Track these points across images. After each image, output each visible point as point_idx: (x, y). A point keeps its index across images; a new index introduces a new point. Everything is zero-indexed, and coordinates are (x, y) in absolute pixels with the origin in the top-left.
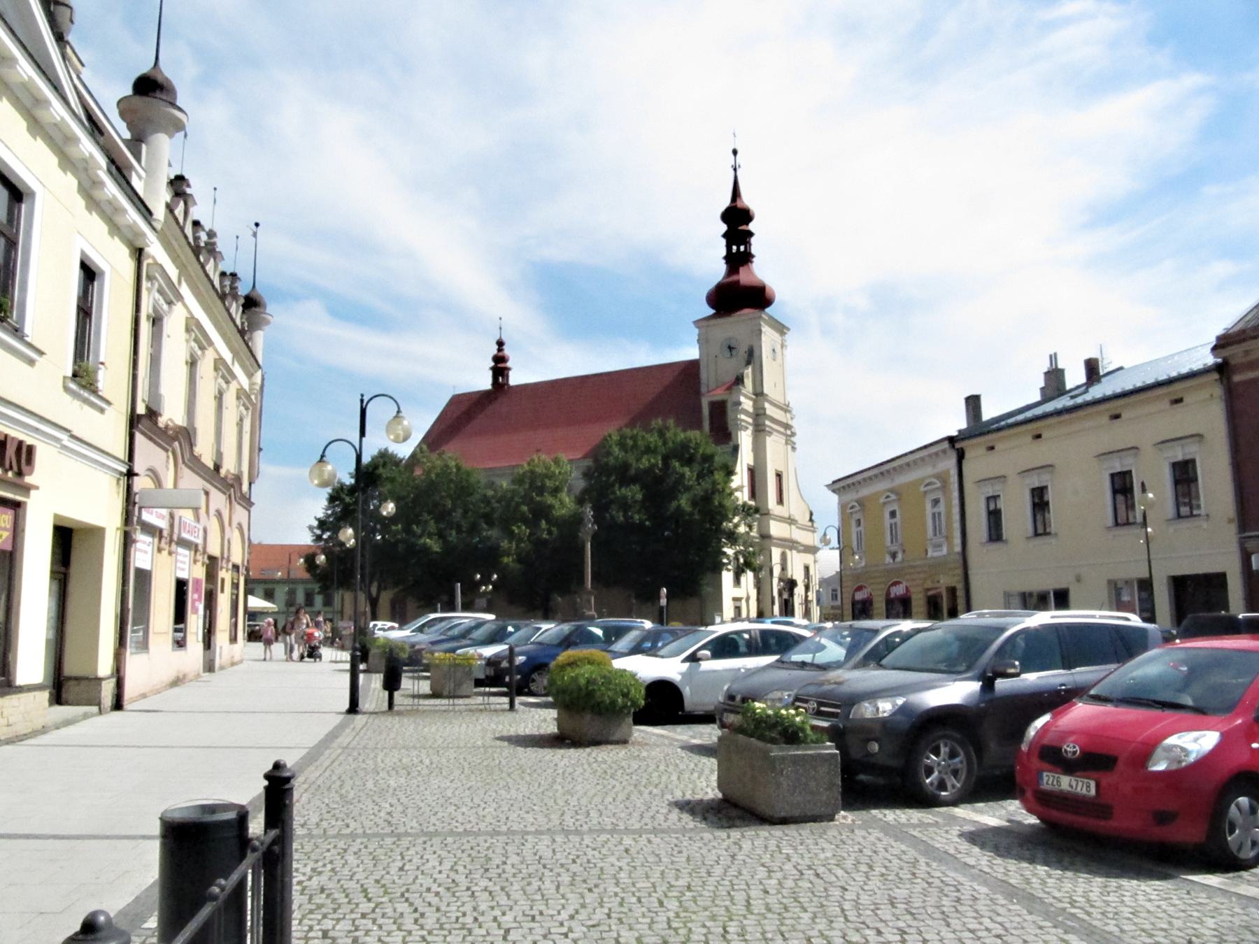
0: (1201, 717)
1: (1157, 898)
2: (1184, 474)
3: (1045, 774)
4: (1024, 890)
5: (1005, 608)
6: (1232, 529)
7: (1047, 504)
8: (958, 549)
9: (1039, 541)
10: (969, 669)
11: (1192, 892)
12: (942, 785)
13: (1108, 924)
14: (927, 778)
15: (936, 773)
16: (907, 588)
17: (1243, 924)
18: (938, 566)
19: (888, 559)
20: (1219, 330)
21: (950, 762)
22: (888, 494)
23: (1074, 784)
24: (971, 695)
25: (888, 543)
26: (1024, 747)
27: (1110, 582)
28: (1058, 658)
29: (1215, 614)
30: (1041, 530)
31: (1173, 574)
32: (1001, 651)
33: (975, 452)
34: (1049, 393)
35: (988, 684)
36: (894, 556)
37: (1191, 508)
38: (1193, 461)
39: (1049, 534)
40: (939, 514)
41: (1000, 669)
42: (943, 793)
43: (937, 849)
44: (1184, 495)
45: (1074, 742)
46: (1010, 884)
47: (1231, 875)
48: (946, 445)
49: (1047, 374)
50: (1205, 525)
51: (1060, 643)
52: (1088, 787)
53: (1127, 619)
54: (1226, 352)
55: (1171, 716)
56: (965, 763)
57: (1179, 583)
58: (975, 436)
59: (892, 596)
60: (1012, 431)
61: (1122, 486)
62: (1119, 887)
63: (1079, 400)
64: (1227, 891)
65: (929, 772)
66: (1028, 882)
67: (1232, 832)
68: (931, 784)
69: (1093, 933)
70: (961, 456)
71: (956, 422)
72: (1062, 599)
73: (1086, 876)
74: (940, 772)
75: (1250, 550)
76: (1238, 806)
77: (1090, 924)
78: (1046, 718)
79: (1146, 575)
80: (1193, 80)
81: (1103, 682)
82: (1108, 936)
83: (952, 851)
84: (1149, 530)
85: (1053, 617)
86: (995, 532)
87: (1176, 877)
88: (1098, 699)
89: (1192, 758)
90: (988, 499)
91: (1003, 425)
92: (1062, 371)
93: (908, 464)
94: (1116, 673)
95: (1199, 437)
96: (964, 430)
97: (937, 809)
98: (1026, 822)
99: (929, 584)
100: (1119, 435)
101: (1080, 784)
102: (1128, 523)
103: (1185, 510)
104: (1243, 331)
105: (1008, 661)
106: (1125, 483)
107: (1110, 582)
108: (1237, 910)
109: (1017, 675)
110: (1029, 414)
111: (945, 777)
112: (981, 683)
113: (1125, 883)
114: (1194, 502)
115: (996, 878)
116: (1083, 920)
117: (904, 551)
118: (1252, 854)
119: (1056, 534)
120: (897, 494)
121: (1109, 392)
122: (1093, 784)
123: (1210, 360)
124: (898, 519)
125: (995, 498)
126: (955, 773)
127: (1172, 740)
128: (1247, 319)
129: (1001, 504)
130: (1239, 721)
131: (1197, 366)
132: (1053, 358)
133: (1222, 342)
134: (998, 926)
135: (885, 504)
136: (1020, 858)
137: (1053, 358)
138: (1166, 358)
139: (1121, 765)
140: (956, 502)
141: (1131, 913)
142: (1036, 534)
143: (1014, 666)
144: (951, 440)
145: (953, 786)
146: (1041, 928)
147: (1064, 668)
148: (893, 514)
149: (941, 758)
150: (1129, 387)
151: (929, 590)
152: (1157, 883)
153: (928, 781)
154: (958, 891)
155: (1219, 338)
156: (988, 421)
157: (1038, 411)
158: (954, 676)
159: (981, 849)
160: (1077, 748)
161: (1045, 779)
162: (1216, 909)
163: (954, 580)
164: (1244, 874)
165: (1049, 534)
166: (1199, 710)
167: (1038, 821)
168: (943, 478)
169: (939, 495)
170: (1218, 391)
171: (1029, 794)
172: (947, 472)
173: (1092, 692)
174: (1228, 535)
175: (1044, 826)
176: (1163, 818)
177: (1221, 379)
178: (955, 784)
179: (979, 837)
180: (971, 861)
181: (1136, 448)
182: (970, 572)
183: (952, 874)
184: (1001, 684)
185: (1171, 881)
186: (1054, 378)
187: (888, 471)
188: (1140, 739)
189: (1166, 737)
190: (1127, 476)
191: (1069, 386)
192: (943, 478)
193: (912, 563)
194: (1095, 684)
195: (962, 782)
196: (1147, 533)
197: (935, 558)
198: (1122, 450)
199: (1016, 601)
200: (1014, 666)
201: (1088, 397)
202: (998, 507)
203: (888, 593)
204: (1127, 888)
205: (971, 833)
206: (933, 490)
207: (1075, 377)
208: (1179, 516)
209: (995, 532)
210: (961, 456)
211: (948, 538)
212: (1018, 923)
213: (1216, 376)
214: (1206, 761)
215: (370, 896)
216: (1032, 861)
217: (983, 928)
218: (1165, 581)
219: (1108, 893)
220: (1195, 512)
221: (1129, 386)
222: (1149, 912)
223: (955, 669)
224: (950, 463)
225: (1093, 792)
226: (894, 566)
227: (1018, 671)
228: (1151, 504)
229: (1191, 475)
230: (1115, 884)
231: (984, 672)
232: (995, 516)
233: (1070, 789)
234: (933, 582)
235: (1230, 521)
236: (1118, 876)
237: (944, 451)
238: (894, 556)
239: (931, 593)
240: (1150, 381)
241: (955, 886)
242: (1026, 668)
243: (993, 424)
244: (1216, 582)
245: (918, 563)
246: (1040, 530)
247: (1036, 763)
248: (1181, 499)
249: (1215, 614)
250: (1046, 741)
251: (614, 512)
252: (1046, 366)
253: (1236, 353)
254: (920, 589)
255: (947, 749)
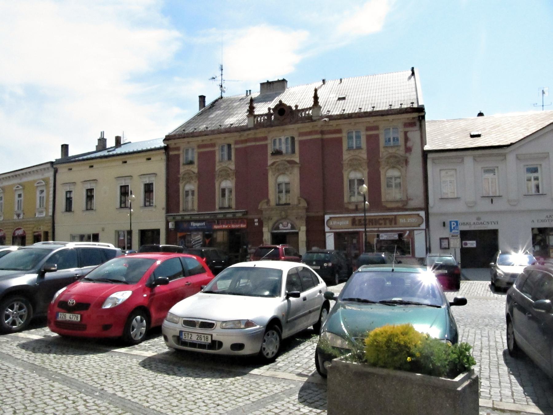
0: (126, 285)
1: (98, 360)
2: (149, 189)
3: (60, 313)
4: (40, 366)
5: (166, 244)
6: (164, 212)
7: (93, 196)
8: (51, 214)
9: (88, 212)
10: (33, 268)
11: (114, 356)
12: (14, 323)
13: (74, 375)
14: (6, 320)
15: (11, 318)
16: (24, 231)
17: (129, 366)
18: (40, 221)
19: (15, 217)
20: (167, 134)
21: (19, 312)
22: (18, 186)
23: (71, 316)
24: (32, 281)
25: (16, 209)
26: (53, 302)
27: (116, 231)
28: (76, 264)
29: (153, 245)
30: (89, 208)
31: (161, 230)
32: (51, 258)
33: (63, 170)
34: (101, 148)
35: (41, 275)
36: (18, 215)
37: (150, 204)
38: (152, 184)
39: (93, 209)
40: (43, 197)
41: (48, 268)
42: (14, 327)
43: (4, 353)
44: (148, 198)
45: (74, 299)
46: (35, 365)
47: (131, 347)
48: (49, 165)
49: (99, 140)
50: (154, 210)
51: (78, 257)
52: (77, 317)
53: (109, 246)
54: (170, 142)
55: (115, 285)
56: (27, 312)
57: (143, 233)
58: (64, 163)
59: (16, 234)
60: (82, 162)
61: (125, 192)
62: (85, 359)
63: (111, 153)
64: (127, 354)
65: (7, 317)
66: (44, 362)
67: (133, 330)
68: (8, 323)
69: (66, 380)
70: (56, 172)
71: (57, 155)
72: (95, 238)
73: (72, 356)
74: (13, 317)
75: (169, 221)
76: (136, 320)
77: (66, 376)
78: (64, 289)
79: (129, 229)
80: (175, 33)
81: (90, 273)
82: (72, 380)
83: (11, 353)
84: (132, 210)
85: (76, 245)
86: (69, 207)
87: (110, 351)
88: (89, 280)
89: (120, 302)
90: (67, 192)
91: (77, 159)
92: (105, 140)
93: (30, 172)
94: (97, 269)
95: (155, 174)
96: (59, 159)
97: (10, 335)
98: (52, 336)
99: (35, 230)
100: (125, 170)
101: (74, 317)
102: (125, 207)
103: (147, 204)
104: (175, 135)
105: (53, 264)
106: (126, 191)
107: (116, 231)
108: (129, 361)
109: (55, 271)
110: (89, 156)
111: (15, 319)
112: (37, 275)
113: (87, 356)
114: (151, 201)
115: (29, 363)
116: (64, 375)
117: (24, 214)
118: (140, 338)
119: (95, 210)
120: (21, 185)
121: (123, 152)
122: (79, 316)
123: (163, 145)
124: (22, 198)
125: (70, 192)
126: (21, 317)
127: (113, 295)
128: (177, 131)
129: (73, 195)
130: (141, 286)
131: (158, 146)
132: (102, 133)
133: (168, 138)
134: (22, 385)
135: (16, 190)
136: (43, 352)
137: (102, 133)
138: (150, 141)
139: (91, 306)
140: (51, 192)
141: (86, 369)
142: (87, 209)
143: (55, 267)
144: (52, 163)
145: (20, 323)
146: (43, 382)
147: (78, 267)
148: (20, 196)
149: (14, 310)
150: (131, 150)
151: (35, 232)
152: (101, 354)
153: (6, 322)
154: (8, 371)
155: (166, 136)
156: (70, 157)
157: (93, 156)
158: (25, 272)
159: (26, 350)
160: (74, 301)
161: (59, 316)
162: (121, 361)
163: (48, 229)
164: (136, 346)
165: (93, 209)
166: (126, 283)
167: (58, 335)
168: (46, 181)
169: (44, 188)
170: (164, 157)
171: (52, 324)
172: (49, 178)
173: (86, 277)
174: (162, 214)
175: (60, 336)
176: (106, 327)
177: (165, 153)
178: (20, 322)
179: (27, 346)
180: (19, 357)
181: (131, 176)
182: (56, 225)
183: (6, 364)
184: (48, 275)
185: (107, 353)
186: (102, 142)
187: (19, 175)
188: (101, 295)
189: (111, 295)
190: (127, 187)
191: (108, 146)
192: (46, 181)
193: (28, 220)
194: (87, 274)
195: (24, 321)
196: (131, 211)
197: (40, 218)
198: (126, 176)
199: (78, 238)
200: (55, 267)
201: (114, 152)
202: (71, 196)
203: (14, 234)
204: (88, 358)
205: (24, 344)
206: (41, 186)
207: (111, 143)
208: (145, 206)
209: (69, 207)
210: (56, 172)
211: (47, 209)
212: (33, 382)
213: (163, 151)
214: (125, 303)
215: (479, 367)
216: (49, 352)
217: (14, 386)
218: (137, 232)
219: (78, 361)
220: (151, 205)
221: (131, 150)
222: (93, 367)
223: (27, 268)
224: (50, 174)
225: (79, 319)
226: (18, 221)
227: (56, 268)
228: (133, 200)
229: (151, 189)
230: (83, 357)
231: (40, 270)
232: (69, 201)
233: (69, 319)
234: (37, 229)
235: (163, 209)
236: (86, 354)
237: (48, 168)
238: (18, 215)
239: (36, 234)
240: (140, 149)
241: (6, 370)
242: (60, 268)
243: (72, 159)
244: (157, 232)
245: (31, 220)
246: (89, 207)
247: (56, 309)
248: (147, 199)
249: (153, 245)
250: (62, 299)
251: (300, 211)
252: (99, 136)
253: (172, 143)
254: (31, 232)
255: (18, 306)
